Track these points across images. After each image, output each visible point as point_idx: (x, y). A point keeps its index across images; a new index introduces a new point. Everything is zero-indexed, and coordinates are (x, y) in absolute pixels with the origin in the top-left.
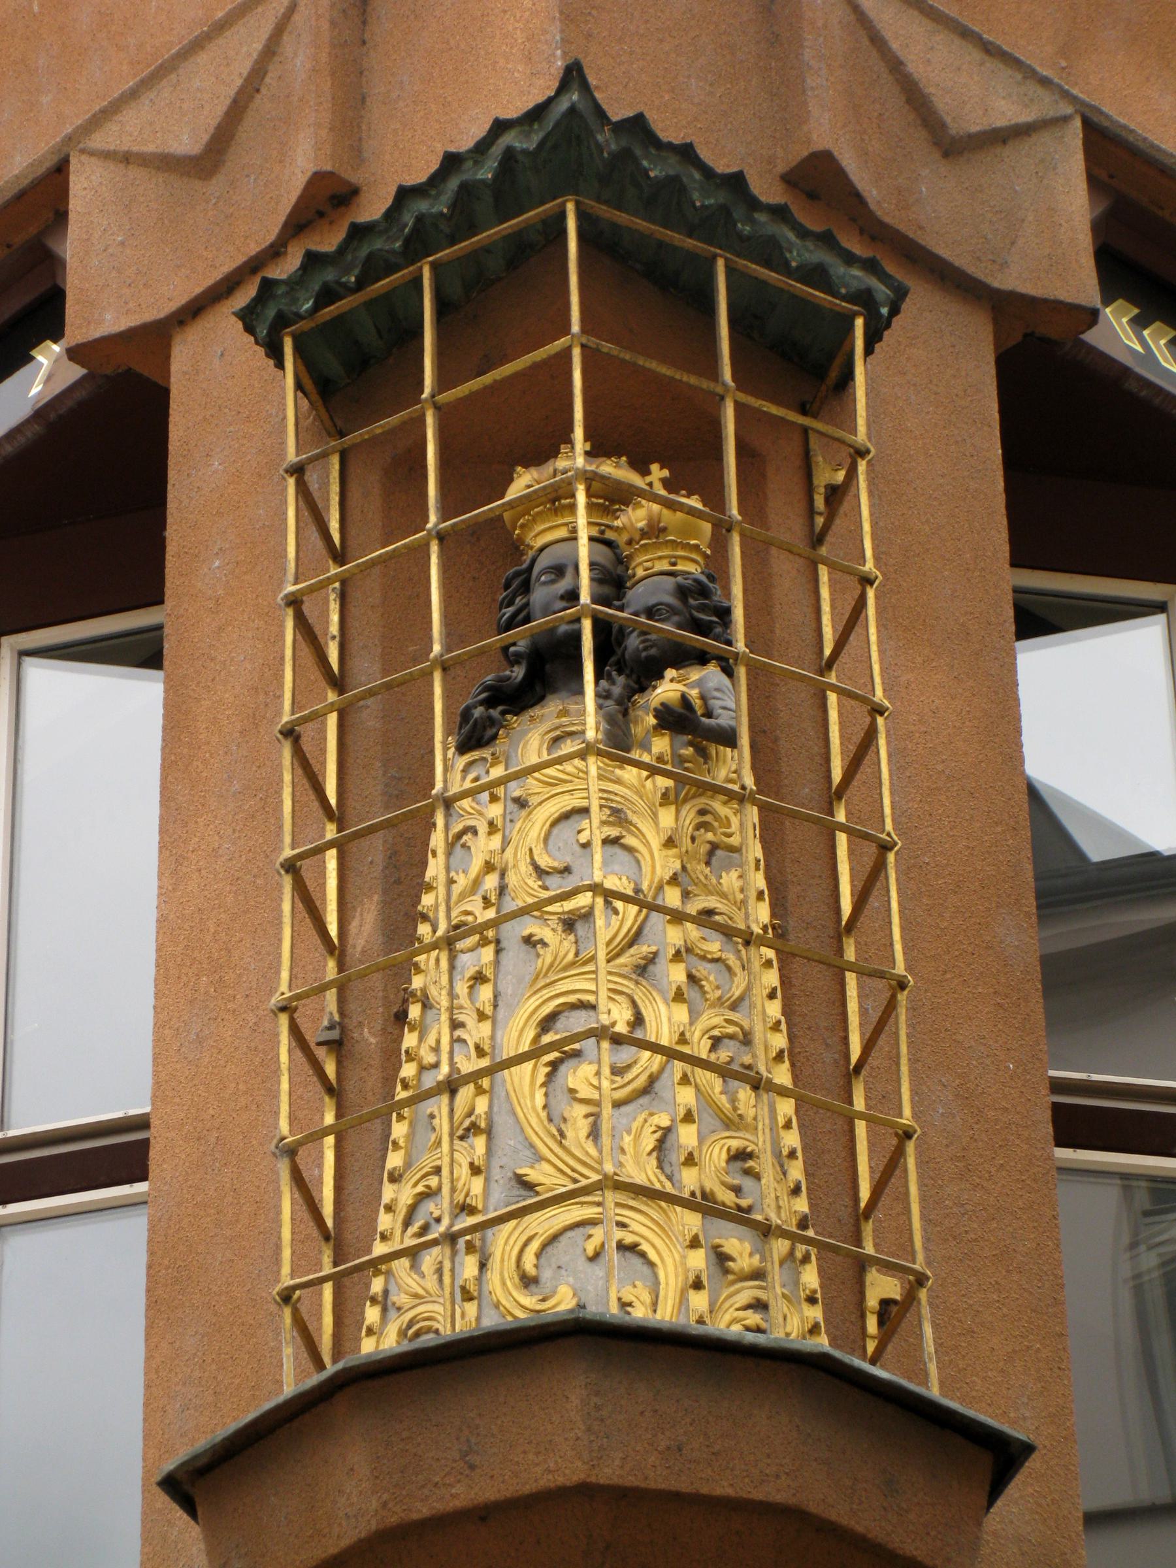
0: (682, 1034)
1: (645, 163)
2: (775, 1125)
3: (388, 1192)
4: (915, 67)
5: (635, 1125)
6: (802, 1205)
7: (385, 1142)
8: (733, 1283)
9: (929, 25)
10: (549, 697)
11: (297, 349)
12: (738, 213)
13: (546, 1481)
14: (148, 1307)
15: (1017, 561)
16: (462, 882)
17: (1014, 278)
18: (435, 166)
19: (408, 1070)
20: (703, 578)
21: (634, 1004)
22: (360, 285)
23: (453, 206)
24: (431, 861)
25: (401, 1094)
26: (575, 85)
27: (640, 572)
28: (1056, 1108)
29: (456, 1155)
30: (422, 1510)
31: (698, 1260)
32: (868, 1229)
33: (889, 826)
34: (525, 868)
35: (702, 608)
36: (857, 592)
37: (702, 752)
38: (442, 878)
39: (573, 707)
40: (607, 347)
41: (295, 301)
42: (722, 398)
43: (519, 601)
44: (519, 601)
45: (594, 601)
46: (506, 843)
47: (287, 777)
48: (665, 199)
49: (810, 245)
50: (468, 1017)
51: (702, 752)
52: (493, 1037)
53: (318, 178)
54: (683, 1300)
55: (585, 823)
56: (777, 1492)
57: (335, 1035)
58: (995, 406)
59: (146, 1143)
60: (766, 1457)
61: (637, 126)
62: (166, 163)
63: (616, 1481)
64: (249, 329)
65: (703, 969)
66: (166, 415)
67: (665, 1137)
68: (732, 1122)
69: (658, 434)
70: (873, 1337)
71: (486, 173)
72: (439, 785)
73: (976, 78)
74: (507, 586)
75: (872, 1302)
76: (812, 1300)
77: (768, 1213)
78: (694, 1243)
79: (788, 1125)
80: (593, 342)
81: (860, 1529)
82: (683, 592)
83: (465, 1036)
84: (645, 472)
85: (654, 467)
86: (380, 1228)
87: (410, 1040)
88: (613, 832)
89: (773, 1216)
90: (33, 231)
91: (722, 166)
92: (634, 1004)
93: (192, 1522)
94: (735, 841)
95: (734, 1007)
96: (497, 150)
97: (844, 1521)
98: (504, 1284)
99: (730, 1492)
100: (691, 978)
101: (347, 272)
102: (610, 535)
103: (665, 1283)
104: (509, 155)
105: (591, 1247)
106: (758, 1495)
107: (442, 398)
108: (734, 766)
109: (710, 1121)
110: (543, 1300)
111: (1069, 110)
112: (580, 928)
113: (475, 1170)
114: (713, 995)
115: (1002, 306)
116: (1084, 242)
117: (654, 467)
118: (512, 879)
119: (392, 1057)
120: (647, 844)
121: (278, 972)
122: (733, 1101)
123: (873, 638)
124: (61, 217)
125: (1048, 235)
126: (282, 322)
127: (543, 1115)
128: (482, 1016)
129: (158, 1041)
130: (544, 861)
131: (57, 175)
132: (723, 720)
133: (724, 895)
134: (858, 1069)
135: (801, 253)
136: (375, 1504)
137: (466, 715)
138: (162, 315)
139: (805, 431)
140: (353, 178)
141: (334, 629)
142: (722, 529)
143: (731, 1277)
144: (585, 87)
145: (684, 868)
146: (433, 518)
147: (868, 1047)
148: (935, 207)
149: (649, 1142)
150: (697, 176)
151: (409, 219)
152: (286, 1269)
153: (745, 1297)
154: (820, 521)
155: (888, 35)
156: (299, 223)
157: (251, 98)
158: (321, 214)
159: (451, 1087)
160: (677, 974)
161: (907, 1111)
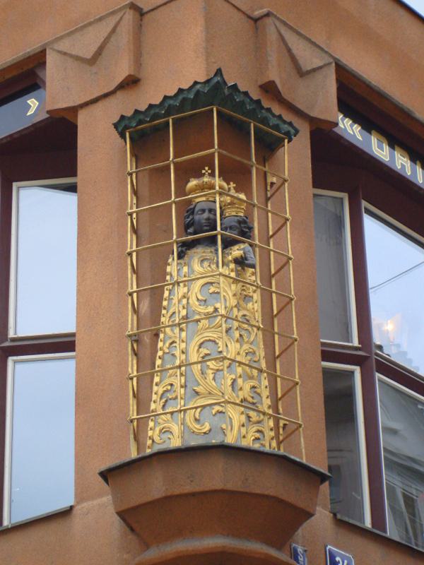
1: (236, 97)
3: (155, 388)
4: (295, 51)
9: (298, 37)
10: (198, 246)
12: (258, 111)
14: (76, 406)
17: (314, 113)
18: (176, 92)
20: (245, 218)
22: (149, 122)
27: (227, 215)
30: (177, 492)
31: (243, 418)
33: (293, 293)
35: (245, 227)
37: (243, 269)
40: (224, 152)
41: (130, 123)
42: (252, 166)
43: (191, 217)
44: (191, 217)
45: (221, 229)
48: (240, 107)
51: (243, 269)
52: (186, 348)
54: (239, 430)
60: (269, 483)
61: (235, 87)
62: (78, 58)
65: (243, 333)
67: (234, 381)
69: (236, 173)
75: (281, 425)
76: (271, 430)
78: (242, 413)
82: (239, 222)
85: (232, 183)
93: (106, 484)
96: (194, 90)
97: (287, 500)
100: (241, 336)
101: (147, 117)
103: (237, 430)
106: (266, 493)
114: (246, 340)
115: (312, 120)
117: (232, 183)
118: (190, 301)
119: (154, 350)
120: (228, 294)
125: (322, 99)
126: (126, 127)
130: (200, 297)
131: (42, 53)
135: (273, 121)
136: (164, 488)
140: (140, 77)
144: (222, 75)
145: (238, 303)
148: (300, 94)
149: (229, 382)
150: (248, 100)
151: (166, 105)
153: (254, 429)
156: (123, 86)
157: (106, 44)
158: (128, 84)
160: (237, 335)
161: (297, 377)
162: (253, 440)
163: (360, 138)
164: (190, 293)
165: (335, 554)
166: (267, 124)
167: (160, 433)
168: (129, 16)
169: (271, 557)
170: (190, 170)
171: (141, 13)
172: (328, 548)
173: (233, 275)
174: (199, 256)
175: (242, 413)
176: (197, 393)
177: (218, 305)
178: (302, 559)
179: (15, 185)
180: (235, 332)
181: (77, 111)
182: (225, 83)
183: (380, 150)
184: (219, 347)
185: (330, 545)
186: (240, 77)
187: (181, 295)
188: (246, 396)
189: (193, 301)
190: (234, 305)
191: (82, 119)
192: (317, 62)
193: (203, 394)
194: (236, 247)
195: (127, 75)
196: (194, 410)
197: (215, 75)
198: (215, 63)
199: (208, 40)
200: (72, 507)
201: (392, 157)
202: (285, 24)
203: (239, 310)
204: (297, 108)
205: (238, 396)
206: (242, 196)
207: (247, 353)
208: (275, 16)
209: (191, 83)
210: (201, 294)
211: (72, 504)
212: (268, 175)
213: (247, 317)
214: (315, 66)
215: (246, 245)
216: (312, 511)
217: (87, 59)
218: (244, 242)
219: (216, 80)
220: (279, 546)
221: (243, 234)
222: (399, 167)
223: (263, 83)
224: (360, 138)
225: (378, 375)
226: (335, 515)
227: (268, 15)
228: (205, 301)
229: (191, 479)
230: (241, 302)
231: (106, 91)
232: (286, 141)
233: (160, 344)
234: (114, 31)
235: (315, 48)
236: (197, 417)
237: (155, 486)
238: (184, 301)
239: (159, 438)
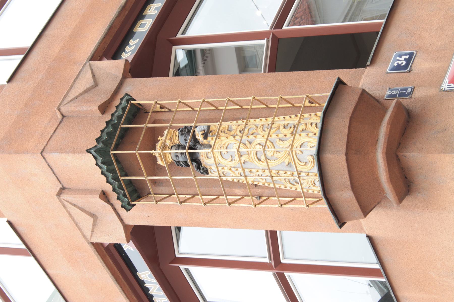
2: (280, 121)
3: (288, 188)
4: (82, 91)
5: (279, 145)
6: (293, 116)
7: (279, 188)
11: (134, 201)
12: (112, 123)
15: (168, 75)
16: (232, 174)
19: (266, 184)
22: (124, 190)
23: (111, 173)
24: (228, 180)
25: (272, 185)
26: (90, 151)
27: (178, 142)
28: (269, 72)
30: (349, 183)
31: (303, 134)
32: (296, 105)
33: (225, 99)
34: (231, 163)
36: (206, 103)
37: (211, 132)
38: (231, 178)
39: (202, 154)
40: (138, 146)
41: (126, 202)
43: (181, 163)
44: (181, 163)
46: (226, 166)
47: (213, 204)
48: (111, 135)
49: (118, 110)
50: (258, 173)
53: (100, 197)
55: (223, 152)
56: (347, 121)
57: (258, 197)
58: (143, 78)
59: (270, 231)
60: (341, 123)
61: (98, 140)
62: (94, 225)
64: (130, 210)
65: (250, 133)
66: (140, 226)
67: (280, 139)
68: (279, 128)
71: (105, 167)
74: (178, 165)
75: (309, 105)
76: (310, 115)
77: (296, 122)
78: (300, 135)
79: (279, 118)
80: (137, 149)
82: (182, 134)
84: (159, 140)
85: (158, 139)
87: (261, 184)
88: (225, 147)
89: (296, 121)
90: (103, 249)
91: (105, 125)
94: (227, 126)
95: (257, 127)
97: (352, 110)
99: (347, 130)
100: (252, 134)
101: (121, 192)
102: (170, 147)
105: (300, 153)
108: (214, 126)
109: (278, 132)
111: (88, 64)
112: (242, 154)
113: (286, 173)
114: (255, 131)
115: (124, 77)
116: (112, 62)
117: (158, 139)
118: (232, 166)
119: (264, 187)
122: (274, 128)
123: (190, 101)
124: (102, 244)
125: (112, 68)
126: (129, 204)
128: (258, 171)
129: (256, 229)
130: (230, 160)
132: (206, 128)
133: (237, 129)
135: (120, 112)
137: (202, 173)
139: (152, 112)
141: (184, 196)
142: (171, 127)
144: (90, 149)
146: (167, 178)
147: (264, 104)
149: (282, 142)
150: (106, 130)
151: (112, 181)
152: (303, 206)
153: (310, 126)
154: (167, 110)
155: (75, 96)
156: (108, 201)
159: (272, 177)
160: (251, 137)
163: (138, 40)
164: (228, 166)
165: (392, 67)
166: (122, 116)
168: (64, 196)
169: (389, 120)
170: (153, 166)
171: (63, 189)
172: (389, 72)
173: (214, 138)
174: (205, 159)
175: (300, 135)
178: (394, 91)
179: (177, 255)
183: (145, 26)
186: (91, 135)
188: (290, 132)
189: (232, 164)
192: (89, 75)
197: (90, 153)
199: (74, 152)
200: (367, 236)
201: (150, 17)
202: (65, 97)
203: (237, 135)
206: (166, 132)
208: (60, 104)
211: (365, 235)
212: (155, 110)
213: (241, 130)
214: (91, 76)
215: (196, 130)
218: (194, 131)
220: (385, 109)
221: (189, 131)
222: (156, 12)
224: (138, 40)
225: (285, 27)
226: (368, 66)
227: (59, 110)
230: (232, 133)
232: (132, 102)
234: (74, 205)
236: (304, 163)
237: (345, 196)
238: (233, 169)
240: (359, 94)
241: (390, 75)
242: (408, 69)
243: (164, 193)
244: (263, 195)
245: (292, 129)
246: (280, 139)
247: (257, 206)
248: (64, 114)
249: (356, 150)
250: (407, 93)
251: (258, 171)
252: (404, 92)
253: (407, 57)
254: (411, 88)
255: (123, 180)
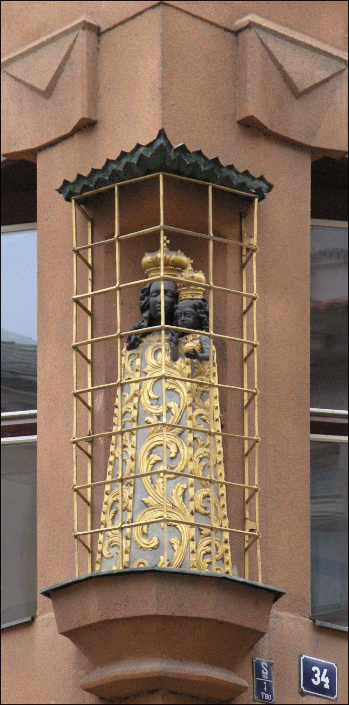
0: (191, 458)
1: (186, 160)
3: (106, 498)
8: (204, 537)
13: (145, 613)
21: (177, 447)
22: (95, 187)
26: (162, 137)
27: (183, 298)
29: (123, 490)
30: (112, 617)
34: (146, 396)
35: (201, 313)
40: (172, 228)
41: (74, 188)
48: (194, 171)
52: (136, 454)
53: (83, 120)
54: (188, 544)
56: (209, 615)
59: (32, 447)
60: (207, 606)
62: (33, 88)
63: (164, 614)
67: (185, 490)
70: (247, 542)
71: (134, 160)
72: (119, 380)
73: (310, 64)
74: (142, 292)
76: (226, 542)
81: (234, 622)
82: (195, 307)
83: (128, 451)
86: (104, 510)
92: (177, 447)
96: (138, 154)
98: (138, 535)
99: (196, 616)
100: (195, 439)
104: (142, 157)
107: (120, 237)
110: (149, 541)
115: (312, 150)
118: (142, 400)
120: (182, 391)
121: (72, 430)
127: (150, 481)
128: (133, 447)
130: (152, 395)
134: (247, 455)
138: (33, 147)
140: (93, 118)
143: (202, 536)
144: (165, 137)
149: (180, 492)
150: (203, 160)
154: (244, 259)
160: (190, 437)
162: (204, 555)
164: (142, 390)
166: (231, 186)
167: (108, 548)
176: (146, 505)
177: (171, 404)
178: (267, 673)
180: (189, 435)
181: (36, 155)
182: (170, 145)
184: (171, 453)
185: (305, 654)
187: (132, 392)
188: (198, 507)
189: (145, 400)
190: (188, 403)
191: (42, 163)
192: (322, 74)
193: (152, 506)
194: (190, 337)
195: (80, 118)
196: (141, 527)
197: (159, 136)
198: (174, 105)
199: (164, 78)
203: (194, 409)
204: (292, 140)
205: (188, 507)
207: (201, 459)
209: (133, 146)
210: (154, 393)
213: (203, 417)
214: (317, 81)
216: (262, 630)
217: (42, 91)
219: (161, 141)
220: (230, 665)
223: (242, 118)
226: (314, 621)
228: (158, 399)
229: (126, 603)
231: (63, 133)
232: (256, 200)
233: (112, 448)
235: (319, 56)
237: (92, 609)
239: (108, 552)
240: (257, 628)
241: (297, 662)
242: (304, 690)
243: (95, 257)
244: (95, 448)
245: (203, 510)
246: (185, 490)
247: (74, 445)
248: (241, 35)
249: (164, 632)
250: (262, 693)
251: (133, 447)
252: (265, 689)
253: (327, 686)
254: (272, 698)
255: (113, 189)
